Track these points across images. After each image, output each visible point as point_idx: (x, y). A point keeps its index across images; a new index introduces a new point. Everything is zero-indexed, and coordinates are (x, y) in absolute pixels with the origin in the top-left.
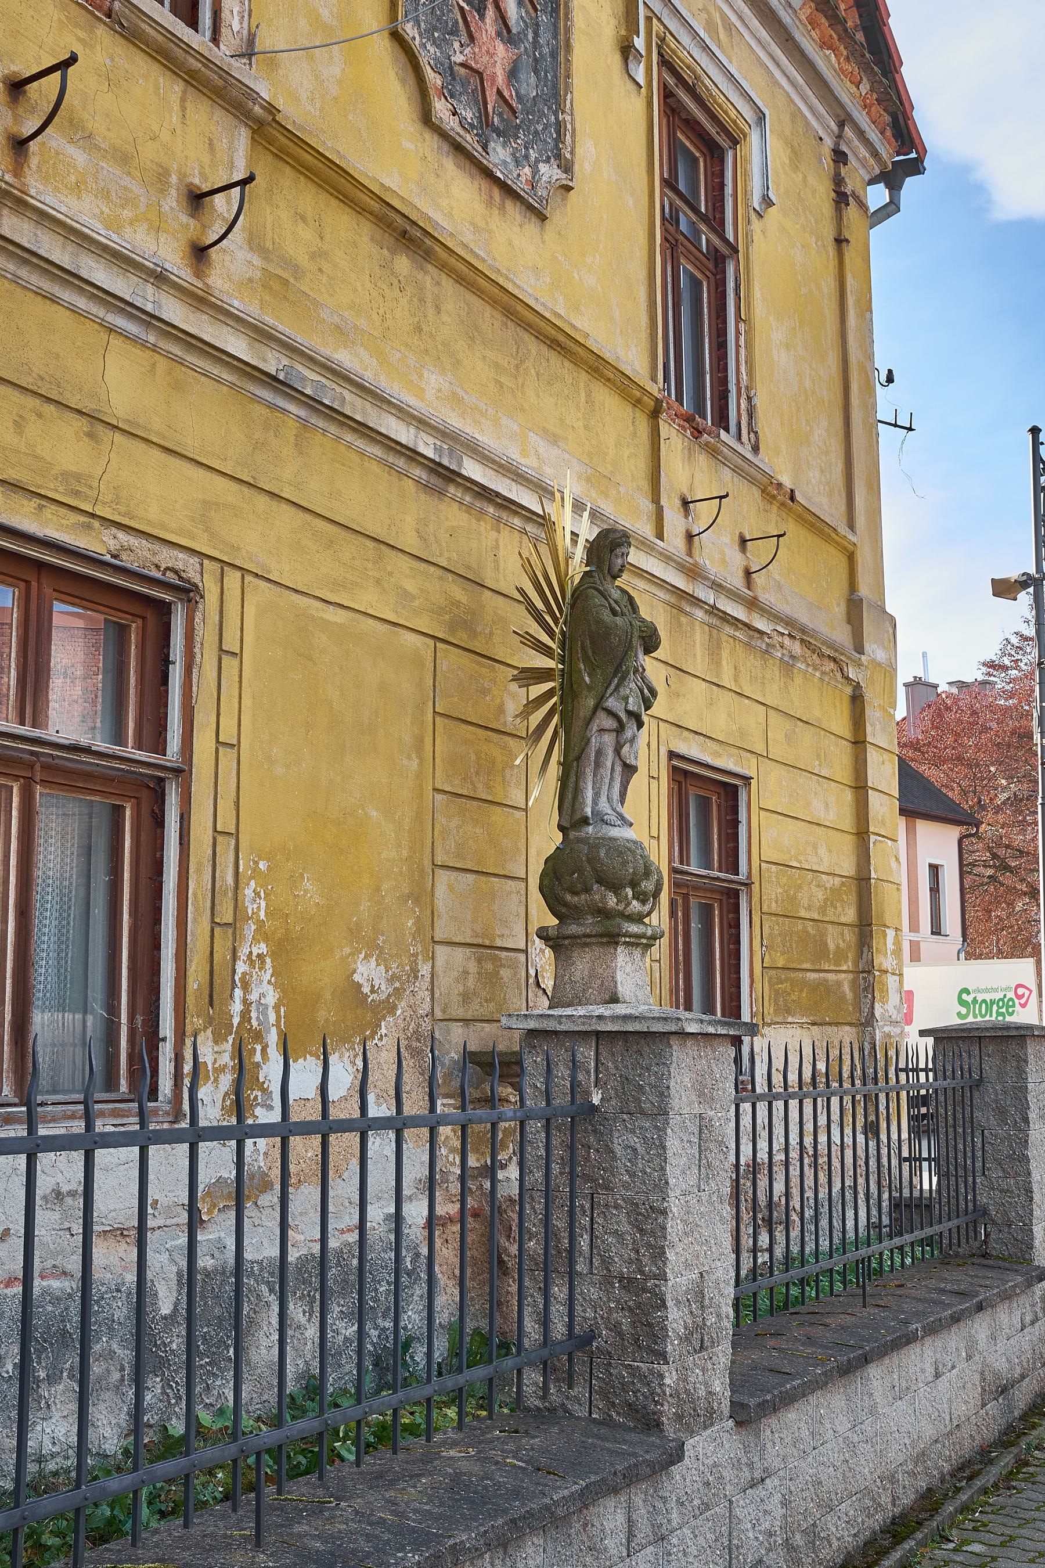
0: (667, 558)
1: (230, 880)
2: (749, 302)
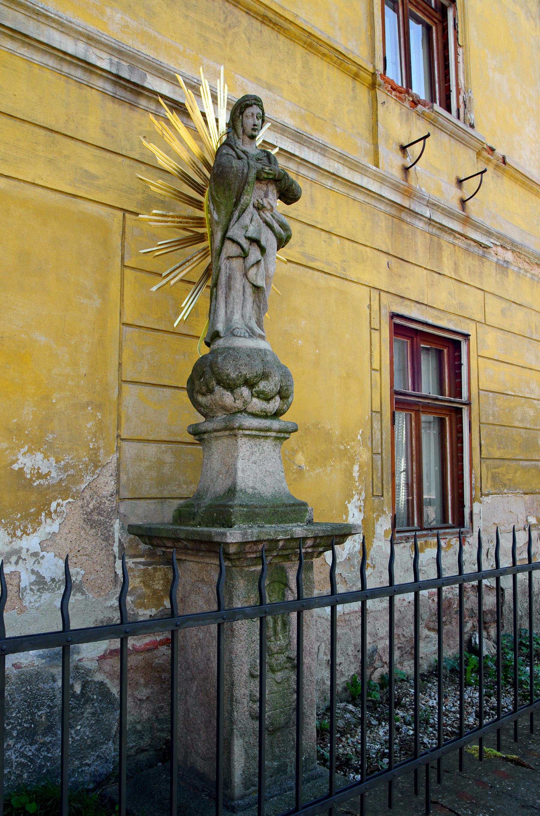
0: (382, 180)
2: (465, 35)
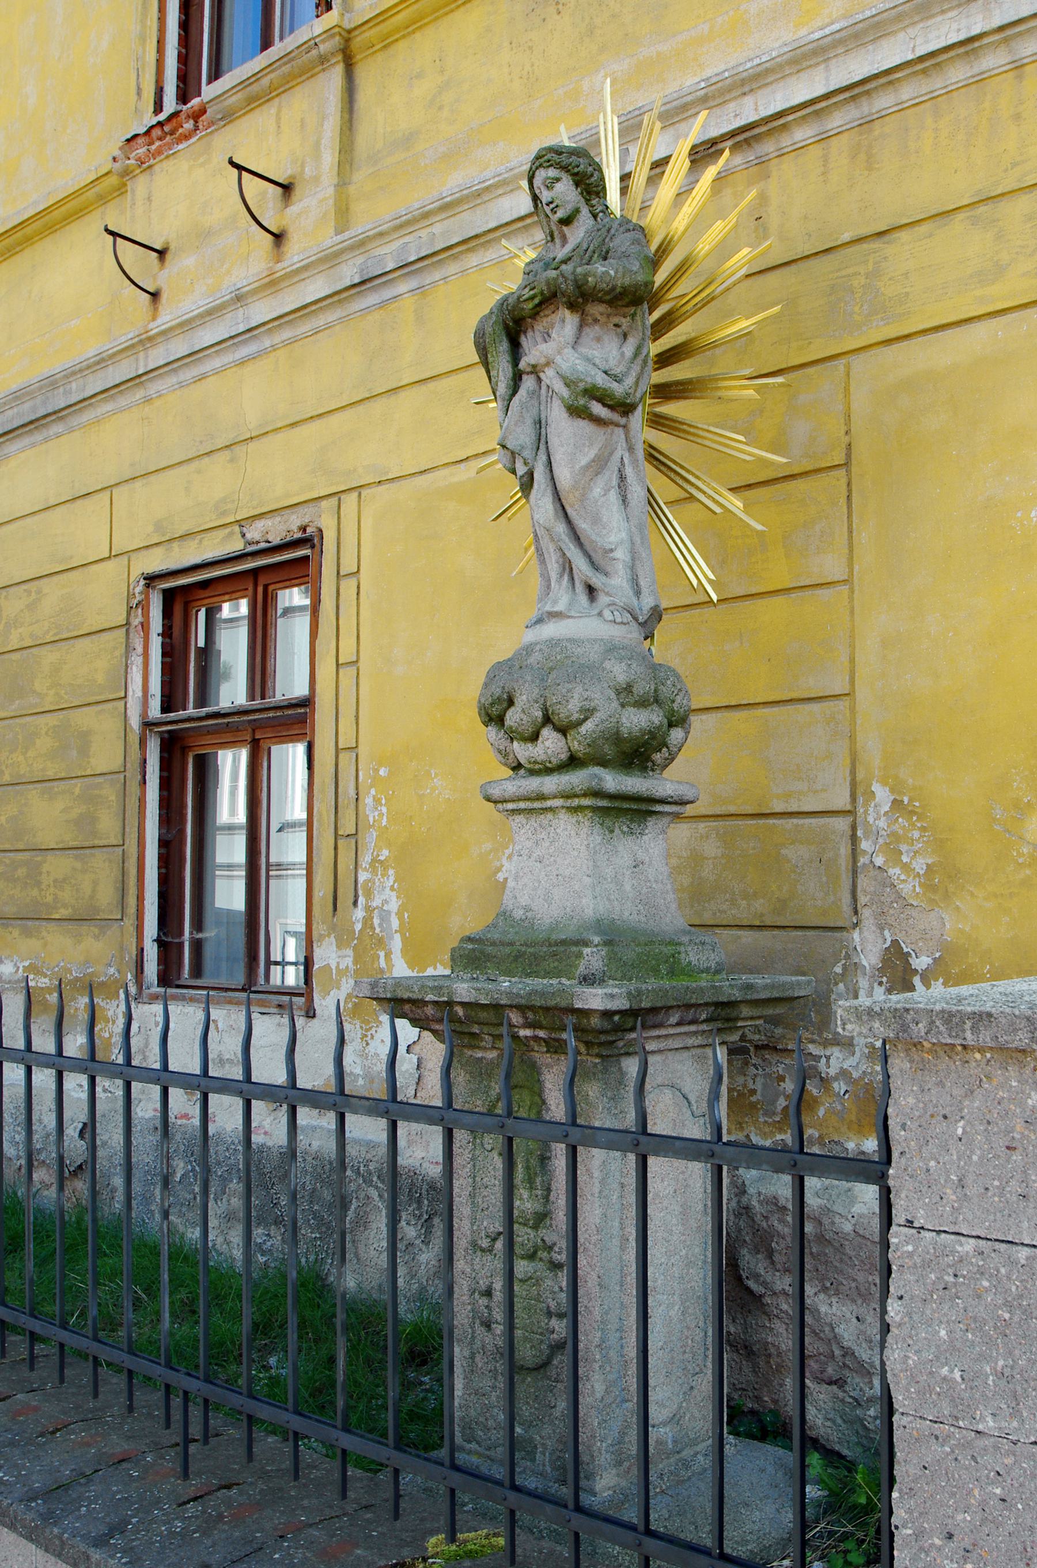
1: (352, 793)
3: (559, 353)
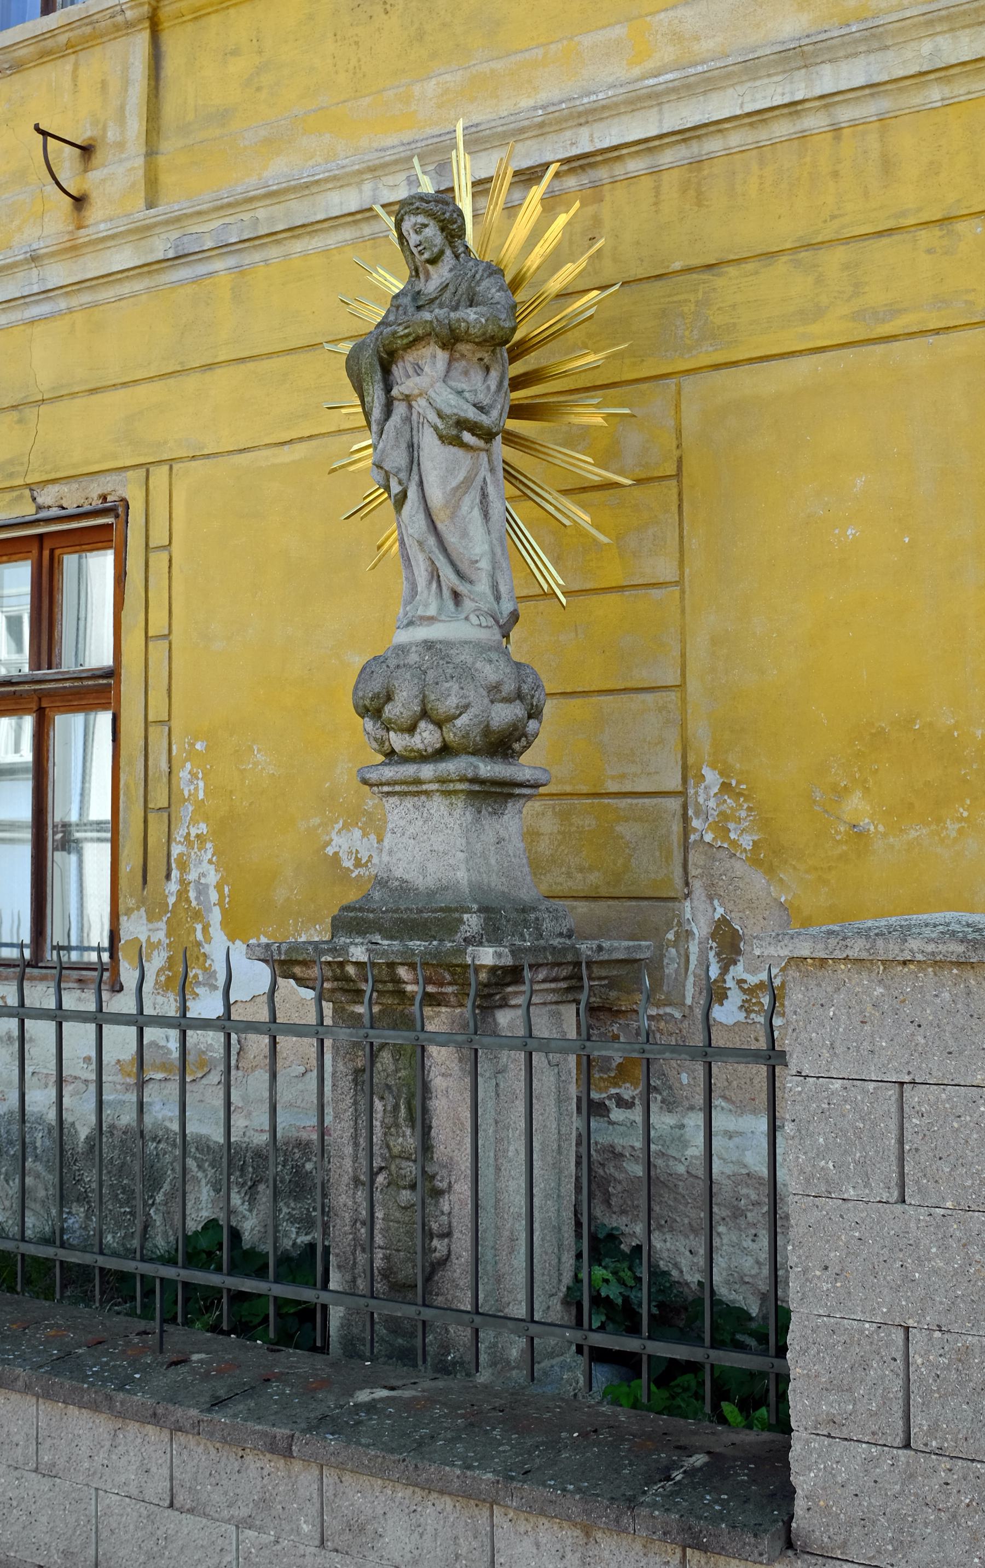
1: (164, 766)
3: (432, 386)
